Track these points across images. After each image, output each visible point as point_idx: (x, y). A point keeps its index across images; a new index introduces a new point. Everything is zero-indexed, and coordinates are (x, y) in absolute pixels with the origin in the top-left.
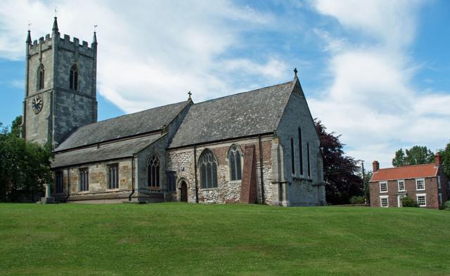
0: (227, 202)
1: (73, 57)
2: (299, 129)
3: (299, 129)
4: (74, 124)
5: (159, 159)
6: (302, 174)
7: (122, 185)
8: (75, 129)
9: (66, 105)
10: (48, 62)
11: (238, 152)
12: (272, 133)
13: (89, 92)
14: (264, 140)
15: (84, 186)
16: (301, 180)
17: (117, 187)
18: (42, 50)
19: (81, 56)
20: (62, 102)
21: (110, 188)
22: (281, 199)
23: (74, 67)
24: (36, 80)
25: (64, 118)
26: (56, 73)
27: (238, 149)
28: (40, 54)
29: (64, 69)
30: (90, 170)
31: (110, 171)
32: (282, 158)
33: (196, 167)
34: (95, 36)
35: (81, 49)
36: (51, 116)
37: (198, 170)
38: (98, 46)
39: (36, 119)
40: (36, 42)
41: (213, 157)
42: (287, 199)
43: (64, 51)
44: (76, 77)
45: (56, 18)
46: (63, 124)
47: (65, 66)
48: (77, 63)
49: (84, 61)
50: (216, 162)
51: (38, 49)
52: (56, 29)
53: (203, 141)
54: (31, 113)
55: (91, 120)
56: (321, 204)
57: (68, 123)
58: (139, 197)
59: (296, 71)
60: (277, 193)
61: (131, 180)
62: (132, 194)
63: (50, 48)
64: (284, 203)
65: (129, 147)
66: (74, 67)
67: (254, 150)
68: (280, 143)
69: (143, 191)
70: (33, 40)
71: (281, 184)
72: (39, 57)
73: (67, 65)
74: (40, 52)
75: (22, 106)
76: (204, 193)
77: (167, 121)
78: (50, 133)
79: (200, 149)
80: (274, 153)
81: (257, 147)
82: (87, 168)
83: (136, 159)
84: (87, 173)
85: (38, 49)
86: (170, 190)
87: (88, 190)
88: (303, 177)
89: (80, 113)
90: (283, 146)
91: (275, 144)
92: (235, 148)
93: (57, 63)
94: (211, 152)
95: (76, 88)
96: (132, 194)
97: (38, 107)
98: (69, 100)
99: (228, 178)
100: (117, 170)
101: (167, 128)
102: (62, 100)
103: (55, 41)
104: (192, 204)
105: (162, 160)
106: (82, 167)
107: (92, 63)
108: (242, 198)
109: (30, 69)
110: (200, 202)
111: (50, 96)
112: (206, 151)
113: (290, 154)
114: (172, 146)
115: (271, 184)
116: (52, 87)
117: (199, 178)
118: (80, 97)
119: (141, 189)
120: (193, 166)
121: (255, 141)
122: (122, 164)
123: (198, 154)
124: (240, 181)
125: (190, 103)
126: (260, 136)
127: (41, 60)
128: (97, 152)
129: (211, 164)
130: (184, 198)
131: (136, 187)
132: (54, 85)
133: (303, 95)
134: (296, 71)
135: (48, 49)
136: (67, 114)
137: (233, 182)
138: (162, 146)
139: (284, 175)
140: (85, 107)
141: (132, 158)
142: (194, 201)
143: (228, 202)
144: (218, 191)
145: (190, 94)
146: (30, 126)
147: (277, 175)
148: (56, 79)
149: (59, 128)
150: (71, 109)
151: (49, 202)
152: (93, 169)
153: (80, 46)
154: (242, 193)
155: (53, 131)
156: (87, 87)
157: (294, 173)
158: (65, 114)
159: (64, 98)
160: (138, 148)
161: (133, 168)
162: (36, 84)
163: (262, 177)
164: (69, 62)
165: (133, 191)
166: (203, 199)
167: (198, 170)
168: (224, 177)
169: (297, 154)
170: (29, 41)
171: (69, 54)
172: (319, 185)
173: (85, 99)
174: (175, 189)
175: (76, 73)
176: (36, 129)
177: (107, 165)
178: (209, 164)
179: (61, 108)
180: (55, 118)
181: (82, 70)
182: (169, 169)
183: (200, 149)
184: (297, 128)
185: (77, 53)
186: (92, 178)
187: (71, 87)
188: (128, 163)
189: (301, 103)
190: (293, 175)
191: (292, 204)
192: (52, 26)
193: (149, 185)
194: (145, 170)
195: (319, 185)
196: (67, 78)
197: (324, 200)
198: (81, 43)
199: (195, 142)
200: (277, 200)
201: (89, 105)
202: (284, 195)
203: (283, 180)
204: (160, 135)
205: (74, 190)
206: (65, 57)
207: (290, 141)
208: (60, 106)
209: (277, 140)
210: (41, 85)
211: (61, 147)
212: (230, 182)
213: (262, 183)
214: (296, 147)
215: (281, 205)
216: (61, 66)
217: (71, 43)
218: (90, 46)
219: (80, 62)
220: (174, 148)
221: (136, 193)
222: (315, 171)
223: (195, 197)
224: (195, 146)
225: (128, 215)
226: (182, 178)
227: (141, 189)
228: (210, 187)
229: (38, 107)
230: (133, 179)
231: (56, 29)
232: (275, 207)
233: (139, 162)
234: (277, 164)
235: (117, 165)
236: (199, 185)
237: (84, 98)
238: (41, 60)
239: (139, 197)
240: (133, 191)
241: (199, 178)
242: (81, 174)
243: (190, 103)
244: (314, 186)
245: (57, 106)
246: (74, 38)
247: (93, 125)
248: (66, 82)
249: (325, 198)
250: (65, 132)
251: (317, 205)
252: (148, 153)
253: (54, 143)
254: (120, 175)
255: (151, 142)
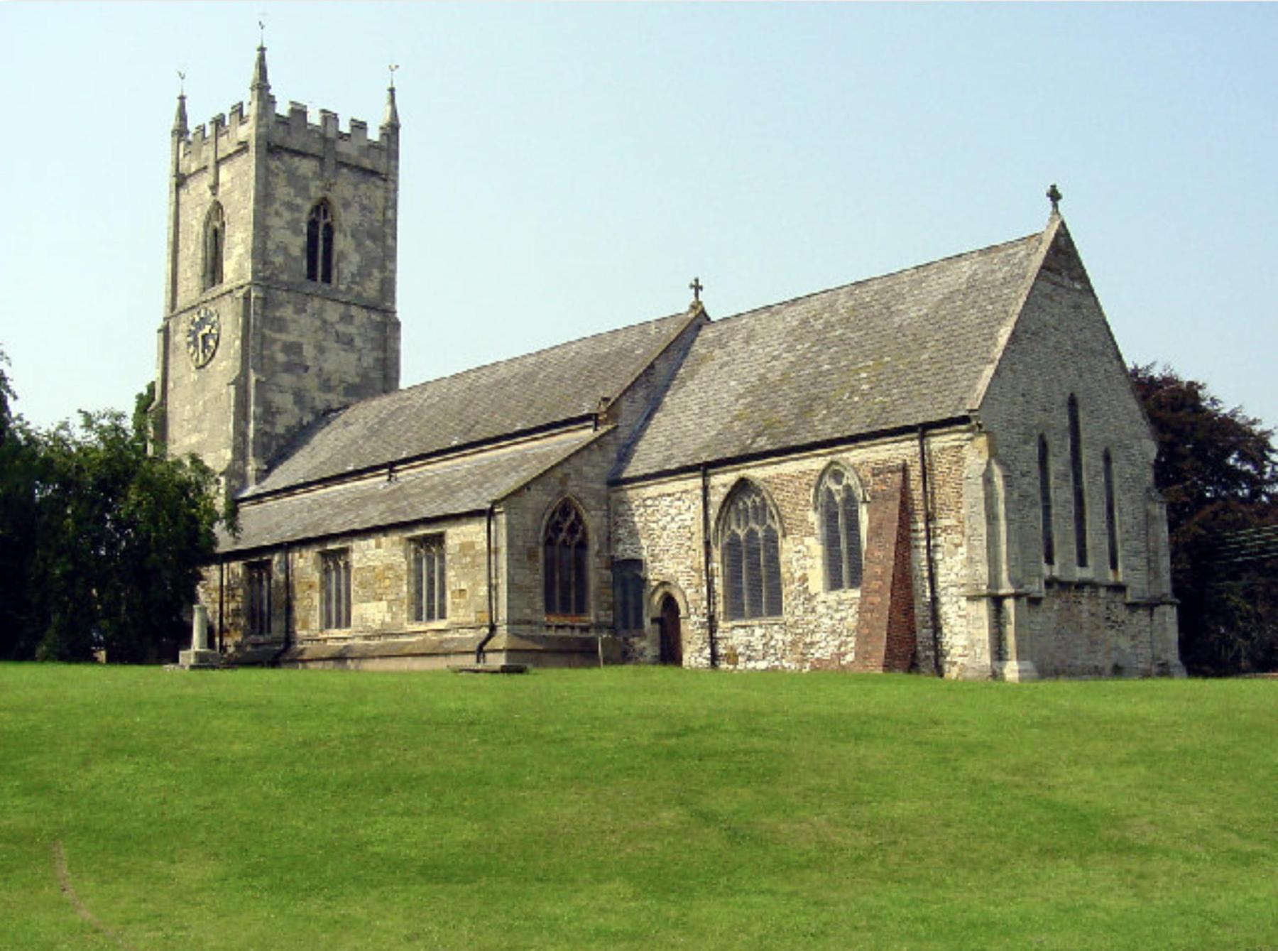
0: (814, 668)
1: (319, 175)
2: (1073, 403)
3: (1073, 403)
4: (321, 399)
5: (585, 516)
6: (1082, 562)
7: (456, 607)
8: (324, 416)
9: (291, 338)
10: (236, 195)
11: (848, 488)
12: (964, 420)
13: (371, 289)
14: (937, 442)
15: (338, 614)
16: (1080, 585)
17: (442, 616)
18: (220, 155)
19: (345, 171)
20: (281, 325)
21: (418, 618)
22: (999, 653)
23: (323, 207)
24: (200, 254)
25: (286, 379)
26: (261, 229)
27: (850, 479)
28: (211, 170)
29: (287, 215)
30: (355, 558)
31: (418, 561)
32: (1001, 508)
33: (707, 544)
34: (262, 59)
35: (343, 147)
36: (244, 374)
37: (717, 554)
38: (402, 133)
39: (200, 386)
40: (202, 129)
41: (764, 505)
42: (1020, 656)
43: (286, 157)
44: (329, 240)
45: (182, 98)
46: (284, 400)
47: (291, 206)
48: (329, 195)
49: (356, 186)
50: (777, 526)
51: (208, 153)
52: (262, 87)
53: (731, 452)
54: (183, 366)
55: (379, 386)
56: (1164, 671)
57: (299, 397)
58: (510, 651)
59: (1054, 195)
60: (984, 634)
61: (483, 590)
62: (489, 637)
63: (243, 147)
64: (1012, 669)
65: (484, 477)
66: (323, 207)
67: (906, 479)
68: (993, 454)
69: (525, 629)
70: (191, 126)
71: (997, 602)
72: (208, 179)
73: (299, 201)
74: (211, 163)
75: (155, 341)
76: (735, 636)
77: (612, 390)
78: (240, 432)
79: (723, 481)
80: (976, 491)
81: (915, 473)
82: (345, 551)
83: (502, 519)
84: (347, 566)
85: (208, 153)
86: (626, 627)
87: (348, 624)
88: (1080, 574)
89: (342, 363)
90: (1002, 463)
91: (975, 455)
92: (838, 476)
93: (264, 197)
94: (757, 491)
95: (327, 278)
96: (489, 637)
97: (206, 346)
98: (304, 320)
99: (817, 581)
100: (442, 558)
101: (613, 408)
102: (280, 319)
103: (258, 127)
104: (695, 671)
105: (593, 520)
106: (421, 532)
107: (380, 194)
108: (862, 655)
109: (182, 220)
110: (724, 665)
111: (240, 309)
112: (743, 486)
113: (1035, 492)
114: (630, 472)
115: (963, 603)
116: (249, 277)
117: (718, 583)
118: (342, 308)
119: (519, 622)
120: (698, 544)
121: (906, 450)
122: (456, 536)
123: (716, 498)
124: (856, 593)
125: (699, 319)
126: (924, 430)
127: (214, 187)
128: (384, 497)
129: (761, 535)
130: (670, 653)
131: (503, 614)
132: (255, 272)
133: (1084, 279)
134: (1054, 195)
135: (238, 152)
136: (296, 366)
137: (833, 597)
138: (595, 470)
139: (1010, 568)
140: (358, 342)
141: (488, 514)
142: (703, 661)
143: (819, 665)
144: (784, 627)
145: (80, 411)
146: (180, 410)
147: (983, 570)
148: (260, 253)
149: (269, 413)
150: (309, 352)
151: (203, 663)
152: (365, 554)
153: (342, 136)
154: (863, 640)
155: (252, 426)
156: (363, 274)
157: (1050, 560)
158: (289, 368)
159: (287, 312)
160: (511, 482)
161: (491, 551)
162: (199, 269)
163: (932, 578)
164: (303, 190)
165: (493, 628)
166: (733, 657)
167: (717, 554)
168: (804, 579)
169: (1062, 495)
170: (181, 132)
171: (306, 167)
172: (1151, 606)
173: (360, 316)
174: (639, 624)
175: (329, 229)
176: (200, 419)
177: (411, 540)
178: (751, 534)
179: (277, 347)
180: (257, 381)
181: (347, 219)
182: (623, 551)
183: (723, 481)
184: (1061, 399)
185: (330, 162)
186: (362, 585)
187: (312, 275)
188: (475, 532)
189: (1077, 307)
190: (1046, 570)
191: (1047, 670)
192: (251, 73)
193: (549, 608)
194: (532, 555)
195: (1151, 606)
196: (297, 244)
197: (1173, 656)
198: (345, 128)
199: (705, 457)
200: (986, 659)
201: (373, 334)
202: (1011, 641)
203: (1006, 589)
204: (591, 431)
205: (305, 626)
206: (293, 178)
207: (1033, 449)
208: (274, 341)
209: (982, 441)
210: (213, 271)
211: (271, 483)
212: (822, 597)
213: (935, 600)
214: (1058, 465)
215: (996, 675)
216: (277, 205)
217: (315, 129)
218: (374, 135)
219: (344, 188)
220: (646, 477)
221: (503, 630)
222: (1136, 553)
223: (707, 651)
224: (705, 469)
225: (558, 732)
226: (663, 584)
227: (519, 622)
228: (756, 614)
229: (206, 346)
230: (492, 588)
231: (262, 87)
232: (965, 686)
233: (509, 523)
234: (983, 530)
235: (439, 539)
236: (720, 608)
237: (354, 310)
238: (214, 187)
239: (510, 651)
240: (493, 628)
241: (718, 583)
242: (326, 572)
243: (699, 319)
244: (1133, 607)
245: (265, 342)
246: (324, 111)
247: (385, 400)
248: (295, 259)
249: (1176, 652)
250: (289, 429)
251: (1146, 675)
252: (540, 499)
253: (252, 467)
254: (450, 575)
255: (553, 460)
